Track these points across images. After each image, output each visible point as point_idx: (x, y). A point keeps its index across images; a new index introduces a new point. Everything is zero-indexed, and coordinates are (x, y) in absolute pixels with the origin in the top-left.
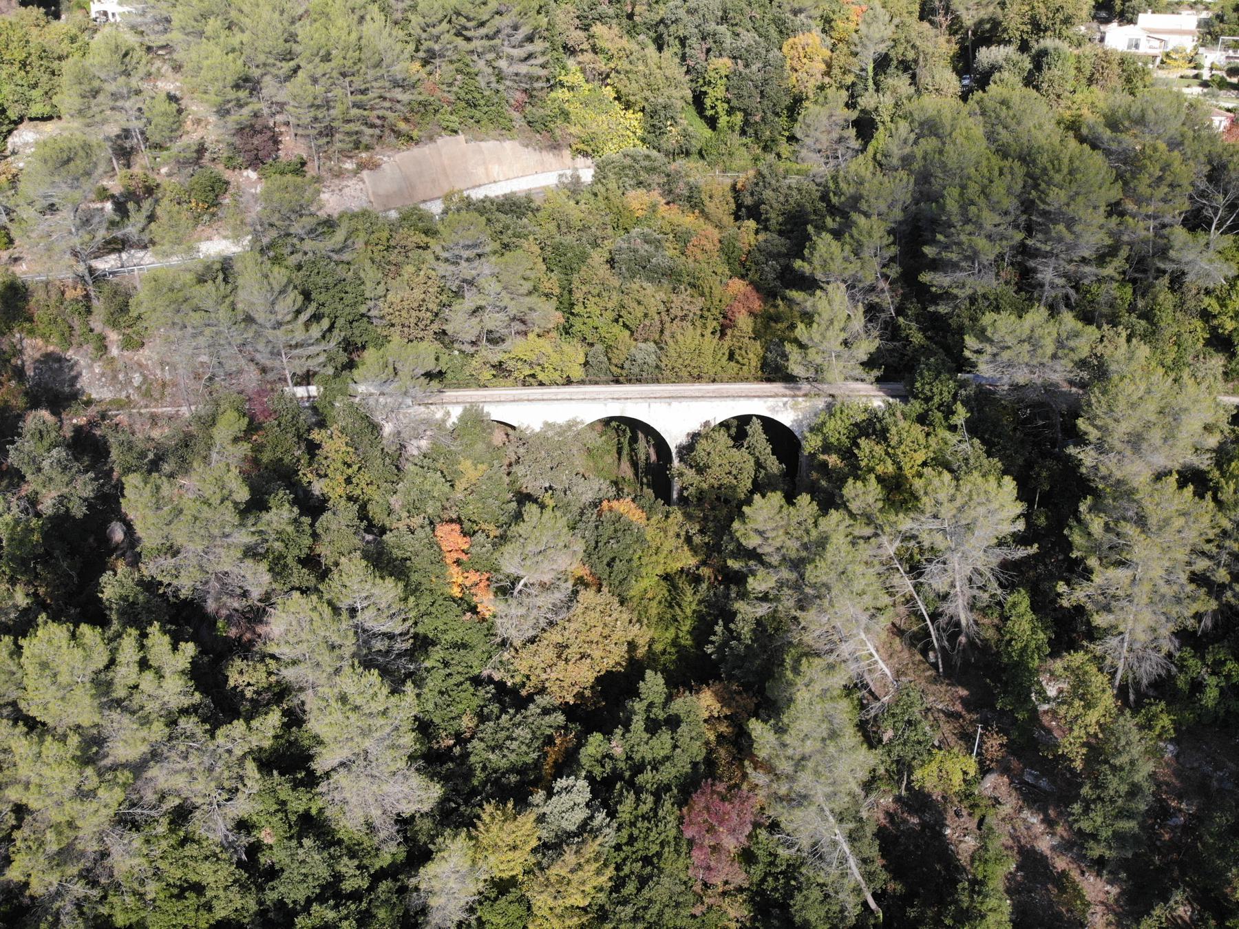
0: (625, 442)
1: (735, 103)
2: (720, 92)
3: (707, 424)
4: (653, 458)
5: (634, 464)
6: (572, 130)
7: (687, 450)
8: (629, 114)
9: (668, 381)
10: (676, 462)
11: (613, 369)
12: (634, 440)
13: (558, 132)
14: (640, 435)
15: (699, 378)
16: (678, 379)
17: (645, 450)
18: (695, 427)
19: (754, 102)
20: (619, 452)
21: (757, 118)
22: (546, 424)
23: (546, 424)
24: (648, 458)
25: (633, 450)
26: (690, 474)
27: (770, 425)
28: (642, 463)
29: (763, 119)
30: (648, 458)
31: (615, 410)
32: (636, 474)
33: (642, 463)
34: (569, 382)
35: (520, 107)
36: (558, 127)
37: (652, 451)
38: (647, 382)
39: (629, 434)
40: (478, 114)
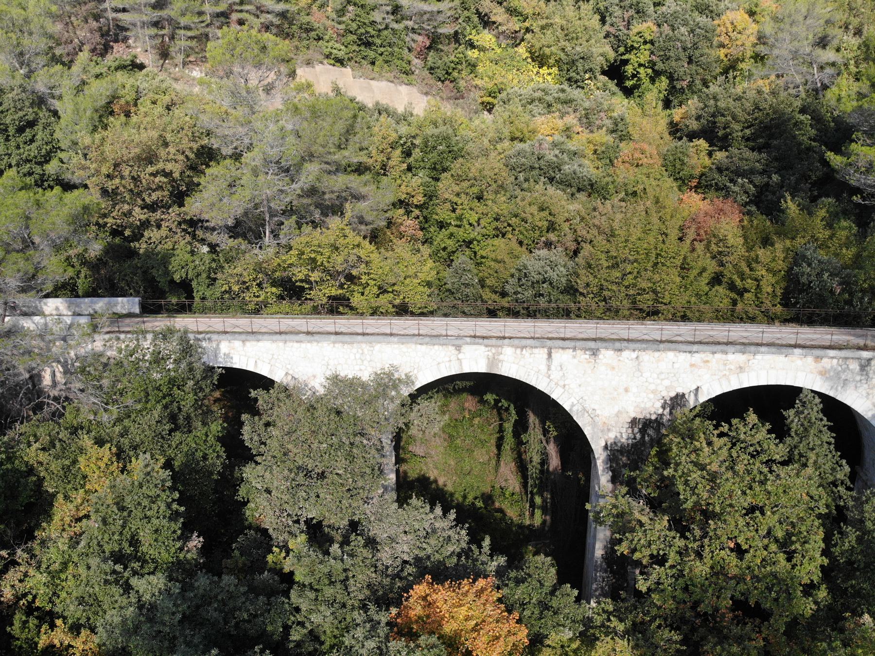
0: (509, 426)
1: (660, 66)
2: (644, 56)
3: (678, 401)
4: (555, 462)
5: (522, 467)
6: (478, 82)
7: (628, 458)
8: (544, 70)
9: (589, 315)
10: (603, 479)
11: (487, 295)
12: (521, 427)
13: (462, 84)
14: (532, 419)
15: (653, 314)
16: (612, 313)
17: (544, 450)
18: (650, 405)
19: (682, 68)
20: (499, 446)
21: (684, 84)
22: (335, 380)
23: (335, 380)
24: (544, 462)
25: (520, 443)
26: (653, 532)
27: (837, 413)
28: (533, 470)
29: (690, 86)
30: (544, 462)
31: (474, 360)
32: (525, 485)
33: (533, 470)
34: (402, 310)
35: (422, 54)
36: (464, 80)
37: (552, 450)
38: (546, 314)
39: (514, 417)
40: (372, 54)
